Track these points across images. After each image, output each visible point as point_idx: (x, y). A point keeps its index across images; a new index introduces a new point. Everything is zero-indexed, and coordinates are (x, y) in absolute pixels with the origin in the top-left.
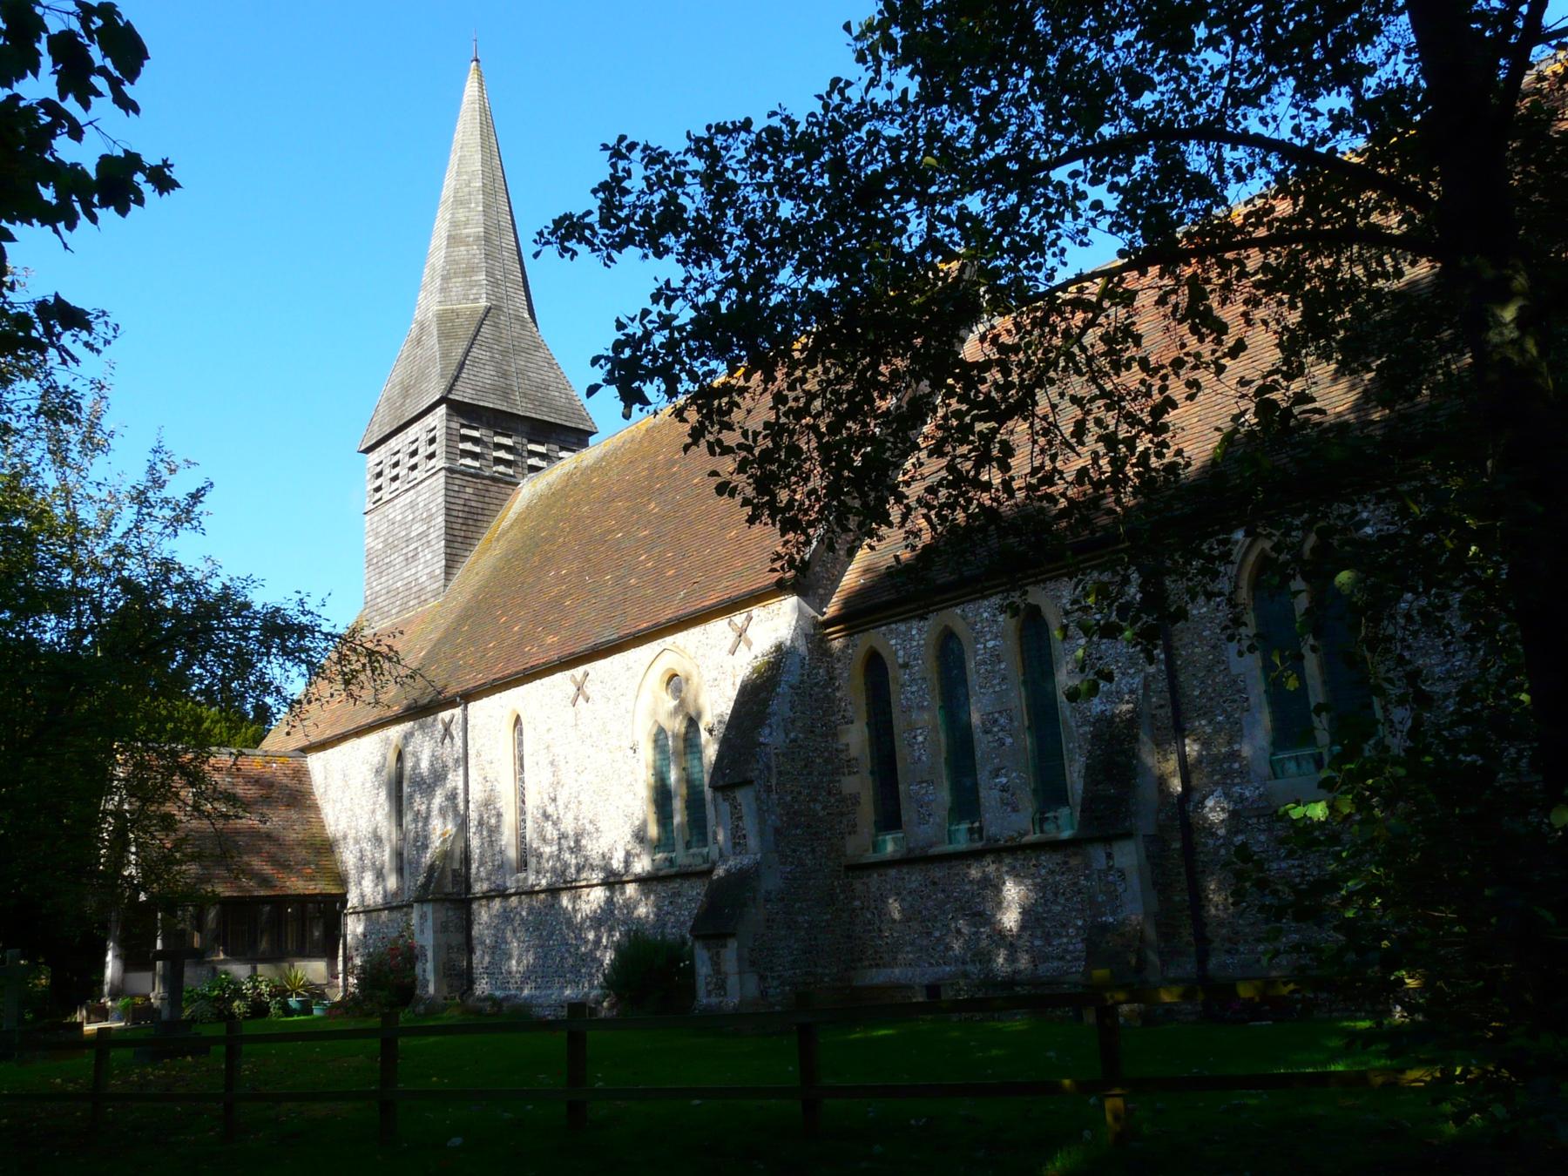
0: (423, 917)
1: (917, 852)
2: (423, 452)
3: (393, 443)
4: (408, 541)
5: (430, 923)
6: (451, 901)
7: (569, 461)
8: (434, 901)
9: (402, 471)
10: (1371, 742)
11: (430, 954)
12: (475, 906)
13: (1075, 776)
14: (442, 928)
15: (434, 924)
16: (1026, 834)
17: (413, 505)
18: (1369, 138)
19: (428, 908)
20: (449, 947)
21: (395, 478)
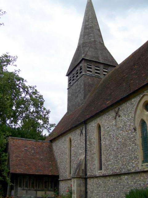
0: (74, 182)
1: (105, 175)
2: (79, 72)
3: (73, 73)
4: (76, 93)
5: (75, 184)
6: (82, 178)
7: (115, 68)
8: (77, 178)
9: (75, 78)
10: (12, 184)
11: (75, 192)
12: (88, 180)
13: (72, 172)
14: (79, 185)
15: (77, 184)
16: (145, 169)
17: (77, 84)
18: (22, 125)
19: (75, 180)
20: (81, 191)
21: (73, 80)
